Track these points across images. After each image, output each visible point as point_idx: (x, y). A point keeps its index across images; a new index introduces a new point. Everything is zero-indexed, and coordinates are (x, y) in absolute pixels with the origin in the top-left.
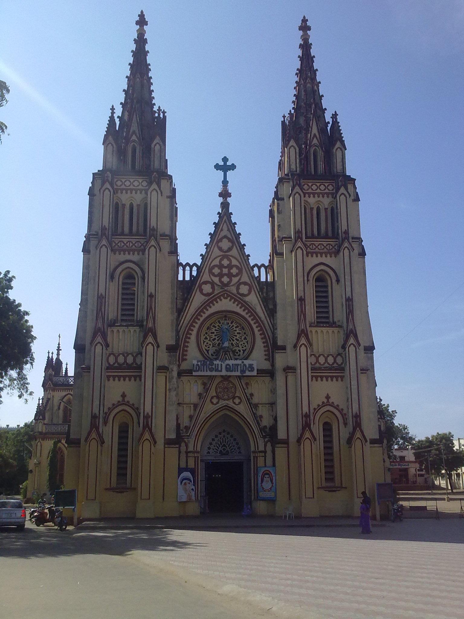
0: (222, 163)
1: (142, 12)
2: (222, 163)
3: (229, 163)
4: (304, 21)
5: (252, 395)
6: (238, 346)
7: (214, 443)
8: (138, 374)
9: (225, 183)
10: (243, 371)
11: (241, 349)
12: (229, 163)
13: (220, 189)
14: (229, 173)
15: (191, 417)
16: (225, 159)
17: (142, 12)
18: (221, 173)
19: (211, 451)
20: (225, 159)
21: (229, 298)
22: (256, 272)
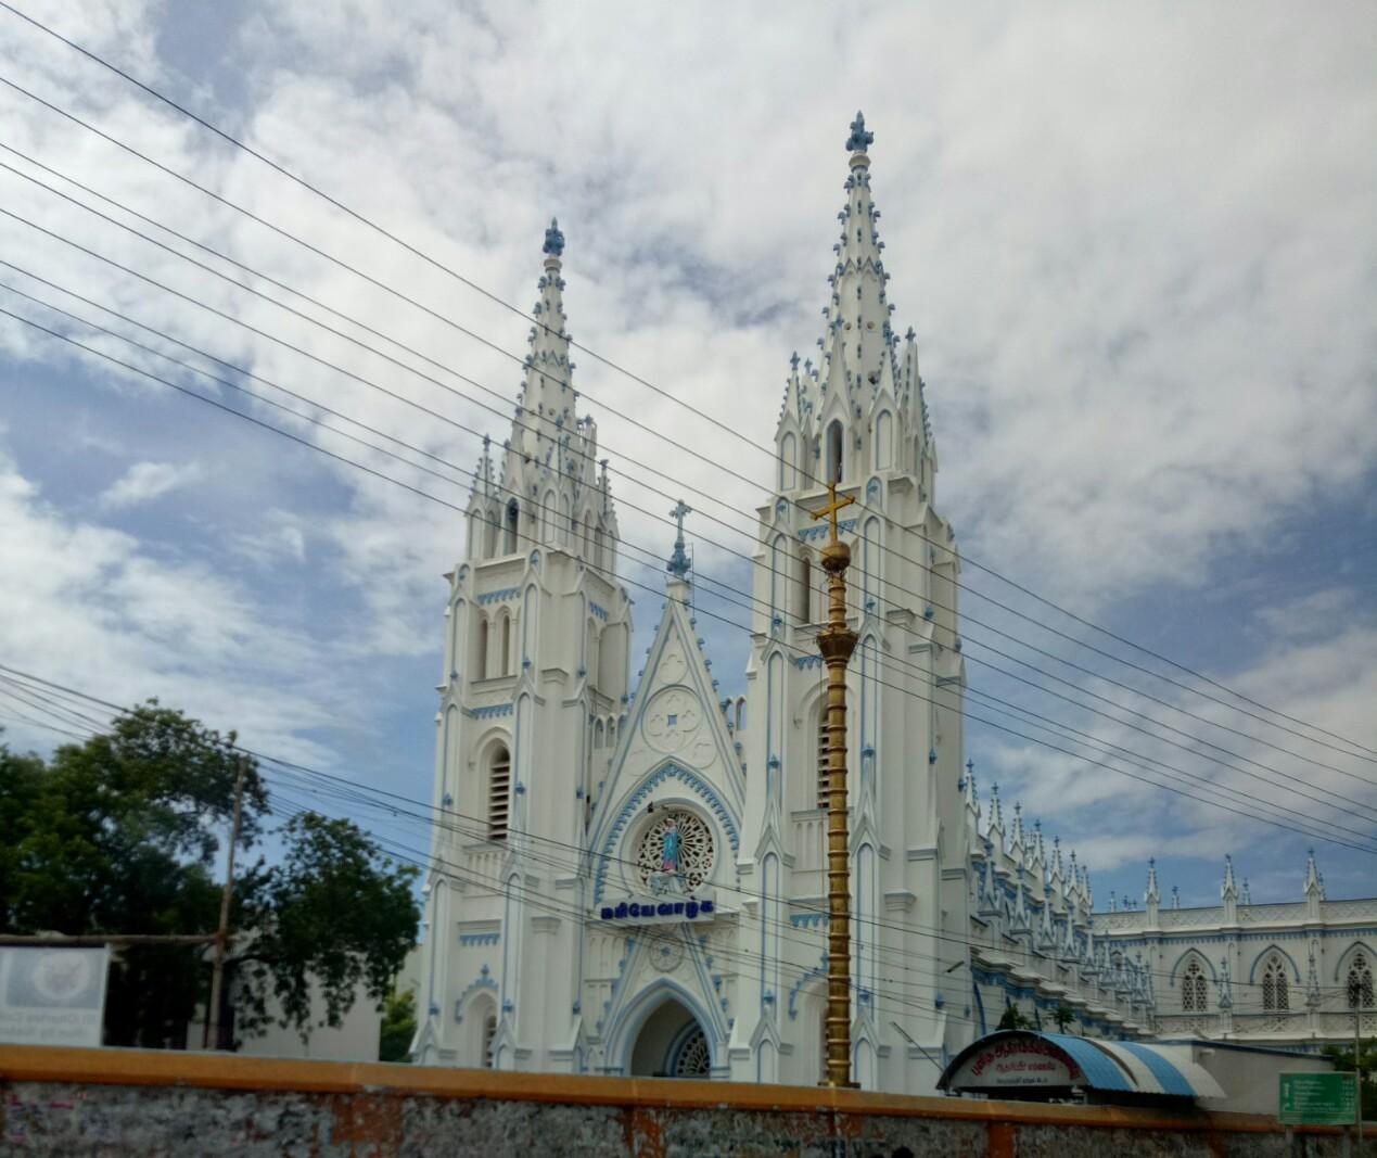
6: (697, 867)
7: (687, 1060)
8: (492, 932)
15: (607, 1006)
17: (860, 115)
19: (685, 1068)
21: (677, 774)
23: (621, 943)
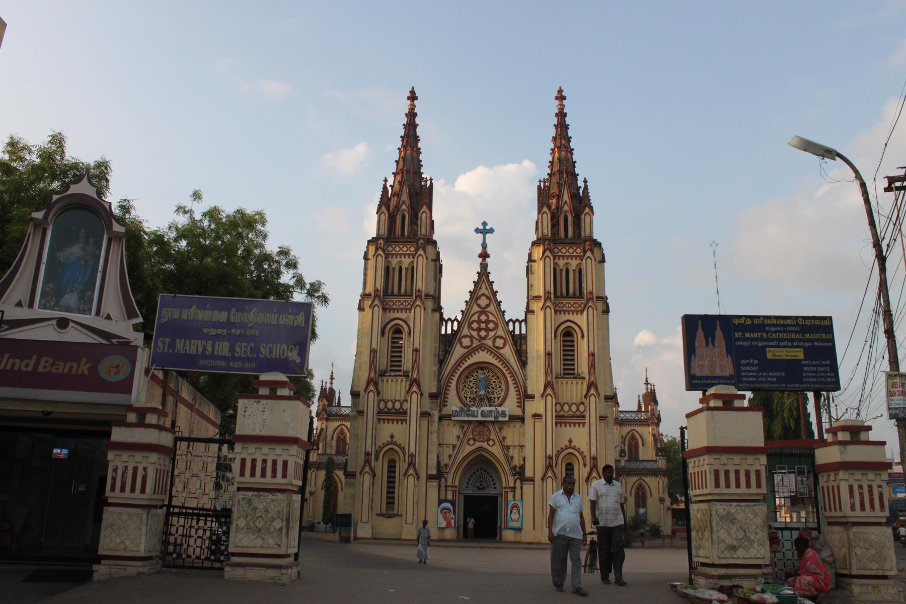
0: (481, 227)
1: (413, 88)
2: (481, 227)
3: (488, 227)
4: (560, 91)
5: (504, 438)
9: (484, 246)
10: (496, 417)
11: (495, 396)
12: (488, 227)
13: (479, 250)
14: (488, 236)
16: (485, 224)
17: (413, 88)
18: (481, 235)
20: (485, 224)
22: (511, 328)
23: (458, 426)
